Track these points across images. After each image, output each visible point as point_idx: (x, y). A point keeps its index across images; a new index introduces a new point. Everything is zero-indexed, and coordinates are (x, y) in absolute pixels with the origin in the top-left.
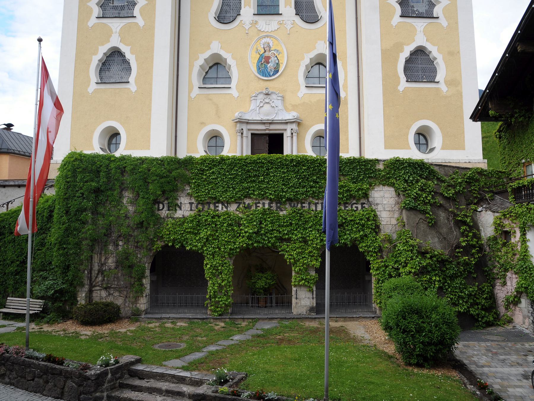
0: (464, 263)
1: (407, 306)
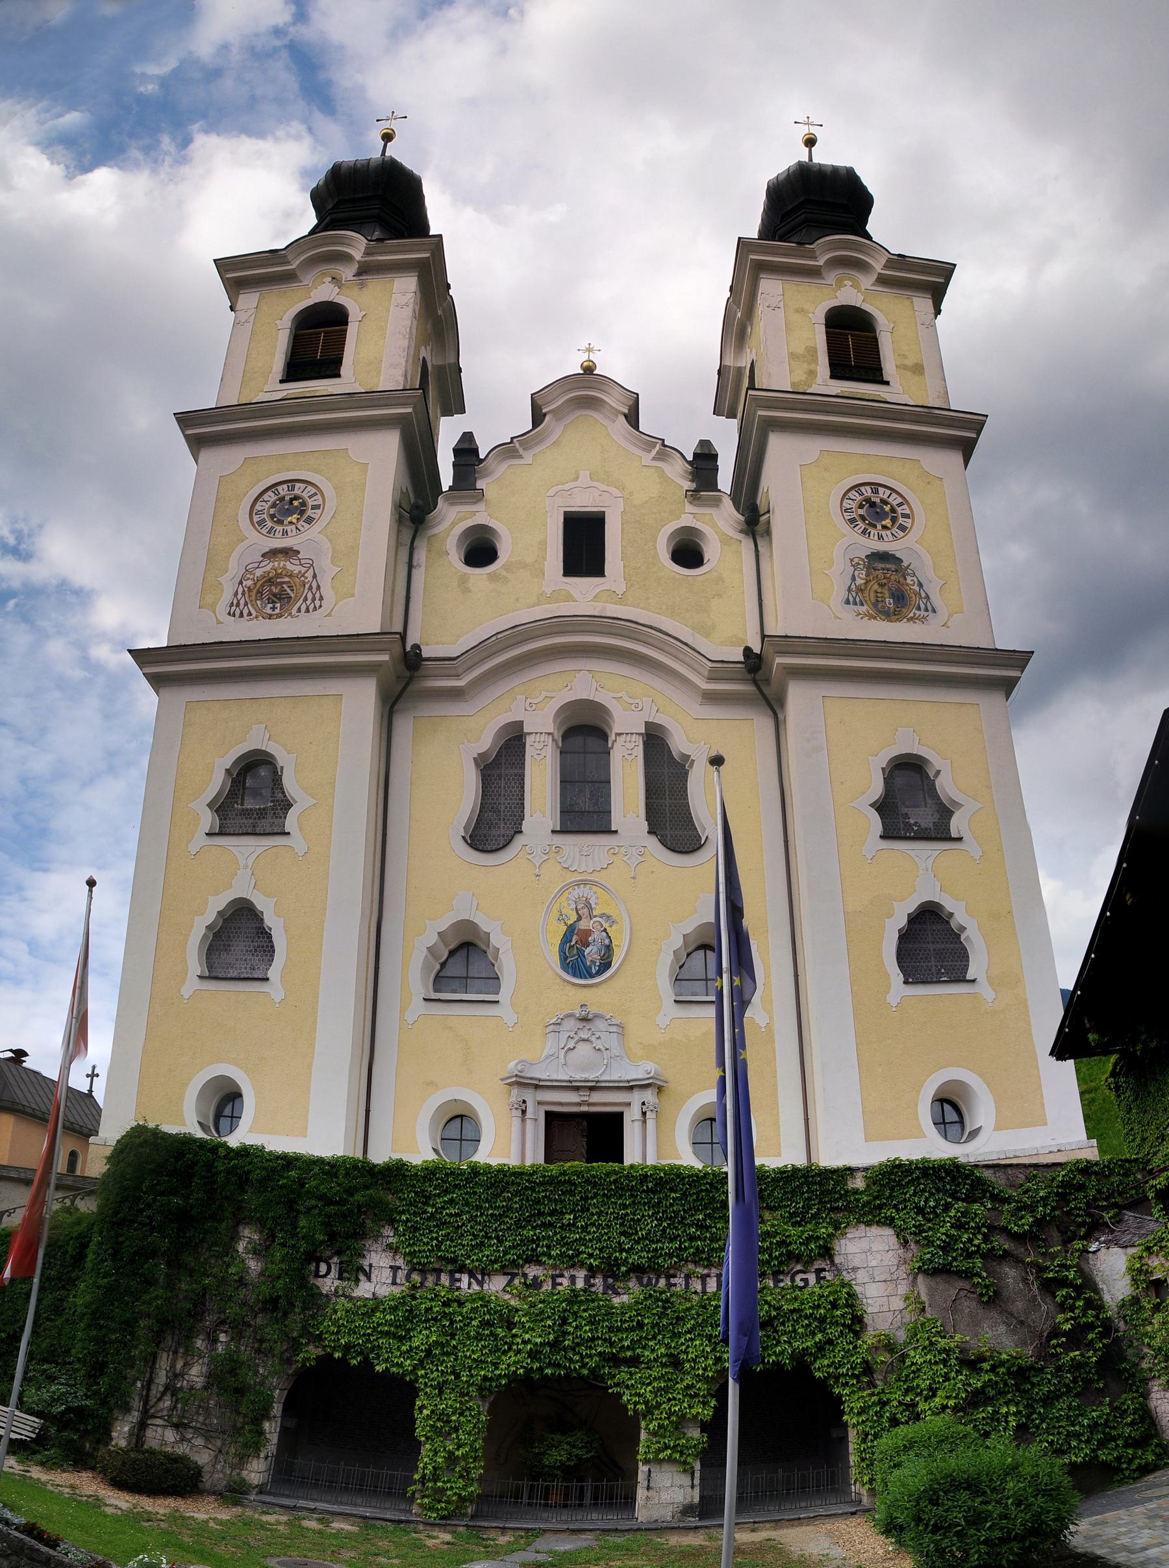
0: (1071, 1366)
1: (942, 1479)
